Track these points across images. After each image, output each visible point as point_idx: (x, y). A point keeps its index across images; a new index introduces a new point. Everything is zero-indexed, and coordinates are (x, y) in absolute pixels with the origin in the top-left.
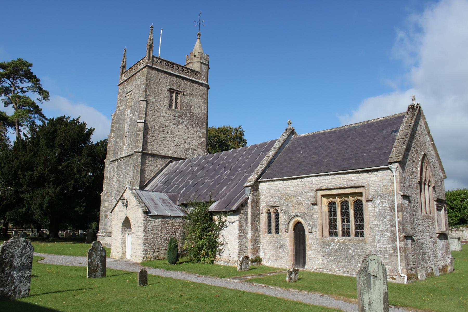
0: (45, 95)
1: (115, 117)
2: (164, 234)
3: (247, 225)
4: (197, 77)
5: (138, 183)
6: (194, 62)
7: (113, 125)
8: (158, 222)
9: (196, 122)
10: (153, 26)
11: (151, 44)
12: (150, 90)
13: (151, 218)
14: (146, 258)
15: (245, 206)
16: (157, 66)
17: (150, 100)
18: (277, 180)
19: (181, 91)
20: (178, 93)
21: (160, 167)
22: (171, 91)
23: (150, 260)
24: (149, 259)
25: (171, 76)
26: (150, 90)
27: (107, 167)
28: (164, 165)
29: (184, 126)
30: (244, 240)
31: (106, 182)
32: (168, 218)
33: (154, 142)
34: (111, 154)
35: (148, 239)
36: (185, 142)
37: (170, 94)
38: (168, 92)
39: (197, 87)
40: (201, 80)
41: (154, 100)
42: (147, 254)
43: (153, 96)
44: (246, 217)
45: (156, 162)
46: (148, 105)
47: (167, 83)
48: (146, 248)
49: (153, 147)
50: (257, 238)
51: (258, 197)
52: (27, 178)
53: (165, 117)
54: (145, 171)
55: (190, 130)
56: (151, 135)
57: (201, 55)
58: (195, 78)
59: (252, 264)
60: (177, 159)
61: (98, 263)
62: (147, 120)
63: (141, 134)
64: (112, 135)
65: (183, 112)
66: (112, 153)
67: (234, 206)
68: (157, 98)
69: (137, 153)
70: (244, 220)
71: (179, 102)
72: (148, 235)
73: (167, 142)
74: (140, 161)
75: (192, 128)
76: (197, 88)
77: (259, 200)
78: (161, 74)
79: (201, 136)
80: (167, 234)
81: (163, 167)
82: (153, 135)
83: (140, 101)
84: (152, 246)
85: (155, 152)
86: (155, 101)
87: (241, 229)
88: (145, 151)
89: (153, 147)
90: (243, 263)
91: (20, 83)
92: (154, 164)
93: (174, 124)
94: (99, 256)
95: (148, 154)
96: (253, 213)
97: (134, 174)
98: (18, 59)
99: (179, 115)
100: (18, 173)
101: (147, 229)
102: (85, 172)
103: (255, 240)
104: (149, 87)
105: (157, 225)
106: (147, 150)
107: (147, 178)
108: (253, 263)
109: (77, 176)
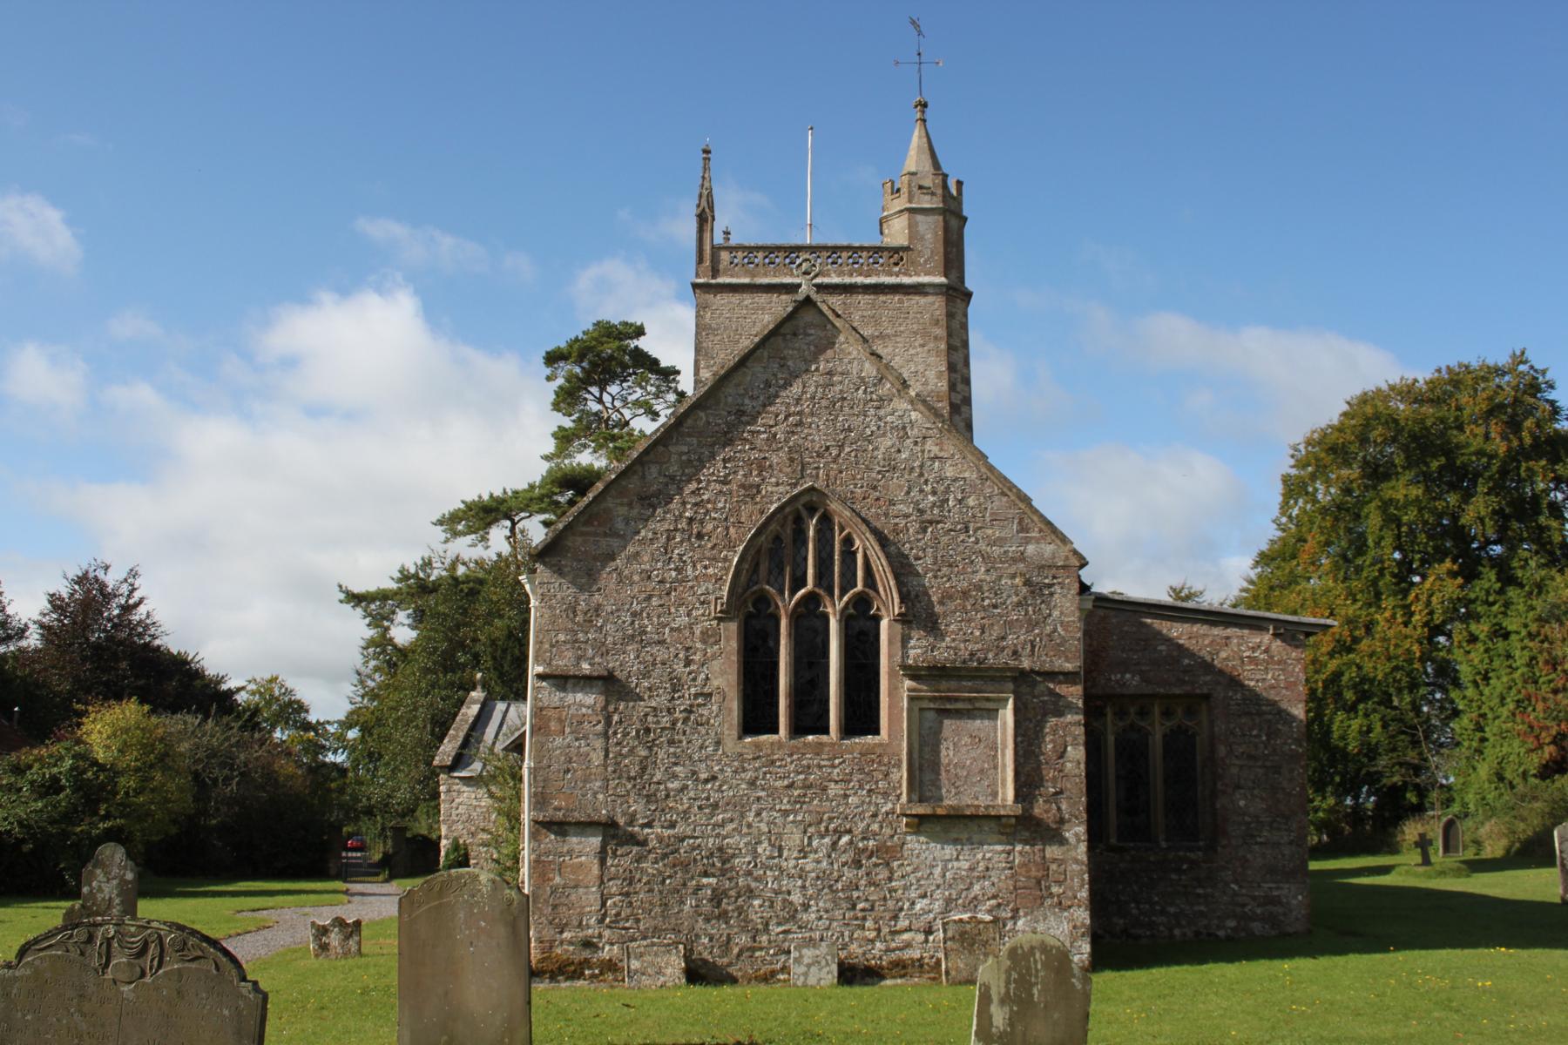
6: (891, 215)
11: (704, 210)
13: (464, 784)
16: (732, 276)
40: (917, 274)
61: (110, 898)
67: (886, 725)
76: (899, 309)
78: (748, 299)
94: (113, 879)
104: (706, 355)
105: (484, 804)
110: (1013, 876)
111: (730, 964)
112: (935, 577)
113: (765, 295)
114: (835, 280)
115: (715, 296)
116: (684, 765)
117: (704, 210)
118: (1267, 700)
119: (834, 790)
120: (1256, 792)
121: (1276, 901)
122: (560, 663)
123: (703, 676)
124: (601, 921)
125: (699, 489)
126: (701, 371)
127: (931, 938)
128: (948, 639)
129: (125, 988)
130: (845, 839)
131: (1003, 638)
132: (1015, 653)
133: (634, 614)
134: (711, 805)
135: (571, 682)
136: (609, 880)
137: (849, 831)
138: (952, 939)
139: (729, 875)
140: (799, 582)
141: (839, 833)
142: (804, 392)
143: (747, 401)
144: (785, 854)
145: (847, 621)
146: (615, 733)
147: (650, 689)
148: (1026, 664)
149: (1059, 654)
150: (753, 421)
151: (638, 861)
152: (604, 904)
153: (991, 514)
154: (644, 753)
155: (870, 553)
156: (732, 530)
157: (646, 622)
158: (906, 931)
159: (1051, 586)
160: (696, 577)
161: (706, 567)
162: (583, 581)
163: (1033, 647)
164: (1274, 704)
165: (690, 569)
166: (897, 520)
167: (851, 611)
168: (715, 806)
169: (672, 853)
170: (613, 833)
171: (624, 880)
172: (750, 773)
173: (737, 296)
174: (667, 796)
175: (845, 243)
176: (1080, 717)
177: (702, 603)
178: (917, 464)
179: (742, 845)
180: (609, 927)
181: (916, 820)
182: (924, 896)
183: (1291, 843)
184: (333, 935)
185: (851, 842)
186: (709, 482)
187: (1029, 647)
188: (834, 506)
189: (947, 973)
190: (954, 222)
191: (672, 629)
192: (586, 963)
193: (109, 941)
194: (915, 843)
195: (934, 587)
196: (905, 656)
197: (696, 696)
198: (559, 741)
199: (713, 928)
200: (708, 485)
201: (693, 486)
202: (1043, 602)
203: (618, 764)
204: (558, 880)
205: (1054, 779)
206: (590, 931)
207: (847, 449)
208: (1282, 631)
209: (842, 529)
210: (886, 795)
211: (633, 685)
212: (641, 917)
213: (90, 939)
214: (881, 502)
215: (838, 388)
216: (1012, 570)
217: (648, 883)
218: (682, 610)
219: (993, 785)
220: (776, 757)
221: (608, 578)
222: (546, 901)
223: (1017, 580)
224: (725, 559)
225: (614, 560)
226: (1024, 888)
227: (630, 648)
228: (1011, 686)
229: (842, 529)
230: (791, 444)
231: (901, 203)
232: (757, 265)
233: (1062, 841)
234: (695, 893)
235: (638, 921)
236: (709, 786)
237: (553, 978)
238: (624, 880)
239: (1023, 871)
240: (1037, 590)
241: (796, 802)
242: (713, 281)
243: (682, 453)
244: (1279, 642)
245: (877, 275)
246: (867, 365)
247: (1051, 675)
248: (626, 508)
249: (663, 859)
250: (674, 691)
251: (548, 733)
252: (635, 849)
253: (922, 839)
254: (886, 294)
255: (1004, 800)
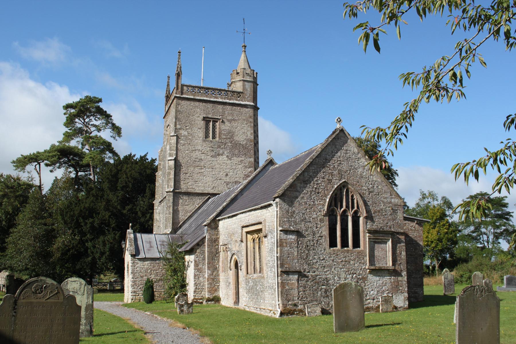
0: (117, 130)
1: (161, 153)
2: (154, 276)
3: (204, 264)
4: (239, 99)
5: (171, 225)
6: (236, 81)
7: (160, 162)
8: (146, 264)
9: (240, 150)
10: (181, 51)
11: (179, 72)
12: (181, 123)
14: (134, 300)
15: (201, 245)
16: (187, 95)
17: (181, 134)
18: (224, 218)
19: (219, 118)
20: (215, 121)
21: (196, 205)
22: (206, 120)
23: (139, 301)
24: (138, 301)
25: (205, 103)
26: (181, 123)
27: (156, 209)
28: (201, 203)
29: (225, 157)
30: (201, 279)
31: (156, 225)
32: (158, 260)
33: (188, 179)
34: (160, 195)
35: (136, 281)
36: (227, 175)
37: (206, 123)
38: (203, 122)
39: (240, 109)
40: (245, 101)
41: (186, 133)
42: (135, 295)
43: (185, 129)
44: (203, 256)
45: (191, 200)
46: (179, 140)
47: (202, 112)
48: (134, 290)
49: (187, 185)
50: (215, 277)
51: (217, 235)
52: (88, 226)
53: (201, 150)
54: (179, 211)
55: (232, 160)
56: (184, 172)
57: (243, 71)
58: (237, 100)
59: (208, 303)
60: (214, 195)
62: (178, 156)
63: (173, 173)
64: (160, 174)
65: (223, 141)
66: (161, 194)
68: (189, 130)
69: (169, 193)
70: (200, 259)
71: (217, 130)
72: (136, 277)
73: (205, 177)
74: (172, 201)
75: (235, 158)
76: (240, 111)
77: (219, 238)
78: (192, 103)
79: (247, 166)
80: (157, 276)
81: (199, 205)
82: (186, 171)
83: (171, 136)
84: (141, 288)
85: (189, 190)
86: (187, 134)
87: (197, 268)
88: (178, 189)
89: (187, 185)
90: (179, 300)
91: (94, 120)
92: (189, 203)
93: (211, 157)
95: (180, 193)
96: (210, 252)
97: (167, 215)
98: (85, 97)
99: (218, 146)
100: (80, 221)
101: (135, 271)
102: (149, 214)
103: (213, 279)
104: (179, 120)
105: (145, 267)
106: (181, 189)
107: (182, 218)
108: (209, 301)
109: (142, 220)
110: (391, 285)
111: (330, 309)
112: (372, 207)
113: (198, 103)
114: (220, 100)
115: (182, 101)
116: (317, 256)
117: (179, 72)
118: (414, 240)
119: (352, 262)
120: (412, 264)
121: (416, 293)
122: (285, 227)
123: (320, 231)
124: (298, 299)
125: (317, 180)
126: (177, 125)
127: (374, 301)
128: (375, 223)
129: (480, 298)
130: (355, 275)
131: (388, 223)
132: (390, 227)
133: (303, 214)
134: (324, 266)
135: (288, 232)
136: (300, 287)
137: (355, 273)
138: (383, 301)
139: (328, 285)
140: (341, 207)
141: (353, 274)
142: (341, 155)
143: (328, 156)
144: (341, 279)
145: (353, 217)
146: (300, 247)
147: (308, 235)
148: (393, 230)
149: (399, 228)
150: (329, 162)
151: (306, 282)
152: (299, 294)
153: (384, 191)
154: (307, 252)
155: (358, 199)
156: (326, 192)
157: (306, 216)
158: (369, 299)
159: (397, 210)
160: (318, 204)
161: (320, 202)
162: (290, 204)
163: (394, 226)
164: (416, 241)
165: (316, 202)
166: (363, 191)
167: (354, 215)
168: (324, 267)
169: (315, 280)
170: (301, 274)
171: (304, 287)
172: (333, 258)
173: (189, 102)
174: (313, 264)
175: (223, 89)
176: (404, 244)
177: (320, 211)
178: (367, 176)
179: (331, 277)
180: (300, 300)
181: (371, 270)
182: (372, 290)
183: (420, 277)
184: (185, 307)
185: (356, 276)
186: (320, 178)
187: (393, 226)
188: (350, 186)
189: (382, 310)
190: (255, 85)
191: (312, 218)
192: (295, 310)
193: (477, 289)
194: (370, 277)
195: (372, 209)
196: (367, 227)
197: (319, 237)
198: (286, 248)
199: (325, 300)
200: (319, 179)
201: (316, 179)
202: (396, 214)
203: (301, 255)
204: (287, 287)
205: (399, 260)
206: (296, 301)
207: (352, 171)
208: (418, 222)
209: (351, 193)
210: (363, 264)
211: (303, 233)
212: (308, 297)
213: (474, 289)
214: (360, 186)
215: (349, 154)
216: (389, 206)
217: (309, 288)
218: (315, 213)
219: (386, 261)
220: (338, 253)
221: (296, 204)
222: (284, 293)
223: (390, 208)
224: (324, 200)
225: (298, 198)
226: (394, 288)
227: (302, 223)
228: (390, 236)
229: (351, 193)
230: (338, 169)
231: (240, 78)
232: (195, 92)
233: (402, 276)
234: (321, 290)
235: (307, 298)
236: (323, 261)
237: (287, 315)
238: (304, 287)
239: (393, 284)
240: (394, 211)
241: (343, 266)
242: (182, 96)
243: (313, 170)
244: (417, 225)
245: (233, 100)
246: (355, 149)
247: (398, 233)
248: (300, 184)
249: (313, 281)
250: (314, 235)
251: (283, 247)
252: (306, 279)
253: (372, 275)
254: (236, 106)
255: (389, 265)
